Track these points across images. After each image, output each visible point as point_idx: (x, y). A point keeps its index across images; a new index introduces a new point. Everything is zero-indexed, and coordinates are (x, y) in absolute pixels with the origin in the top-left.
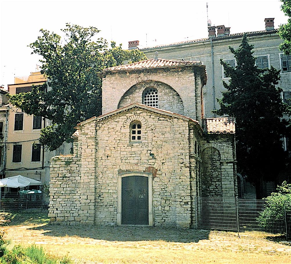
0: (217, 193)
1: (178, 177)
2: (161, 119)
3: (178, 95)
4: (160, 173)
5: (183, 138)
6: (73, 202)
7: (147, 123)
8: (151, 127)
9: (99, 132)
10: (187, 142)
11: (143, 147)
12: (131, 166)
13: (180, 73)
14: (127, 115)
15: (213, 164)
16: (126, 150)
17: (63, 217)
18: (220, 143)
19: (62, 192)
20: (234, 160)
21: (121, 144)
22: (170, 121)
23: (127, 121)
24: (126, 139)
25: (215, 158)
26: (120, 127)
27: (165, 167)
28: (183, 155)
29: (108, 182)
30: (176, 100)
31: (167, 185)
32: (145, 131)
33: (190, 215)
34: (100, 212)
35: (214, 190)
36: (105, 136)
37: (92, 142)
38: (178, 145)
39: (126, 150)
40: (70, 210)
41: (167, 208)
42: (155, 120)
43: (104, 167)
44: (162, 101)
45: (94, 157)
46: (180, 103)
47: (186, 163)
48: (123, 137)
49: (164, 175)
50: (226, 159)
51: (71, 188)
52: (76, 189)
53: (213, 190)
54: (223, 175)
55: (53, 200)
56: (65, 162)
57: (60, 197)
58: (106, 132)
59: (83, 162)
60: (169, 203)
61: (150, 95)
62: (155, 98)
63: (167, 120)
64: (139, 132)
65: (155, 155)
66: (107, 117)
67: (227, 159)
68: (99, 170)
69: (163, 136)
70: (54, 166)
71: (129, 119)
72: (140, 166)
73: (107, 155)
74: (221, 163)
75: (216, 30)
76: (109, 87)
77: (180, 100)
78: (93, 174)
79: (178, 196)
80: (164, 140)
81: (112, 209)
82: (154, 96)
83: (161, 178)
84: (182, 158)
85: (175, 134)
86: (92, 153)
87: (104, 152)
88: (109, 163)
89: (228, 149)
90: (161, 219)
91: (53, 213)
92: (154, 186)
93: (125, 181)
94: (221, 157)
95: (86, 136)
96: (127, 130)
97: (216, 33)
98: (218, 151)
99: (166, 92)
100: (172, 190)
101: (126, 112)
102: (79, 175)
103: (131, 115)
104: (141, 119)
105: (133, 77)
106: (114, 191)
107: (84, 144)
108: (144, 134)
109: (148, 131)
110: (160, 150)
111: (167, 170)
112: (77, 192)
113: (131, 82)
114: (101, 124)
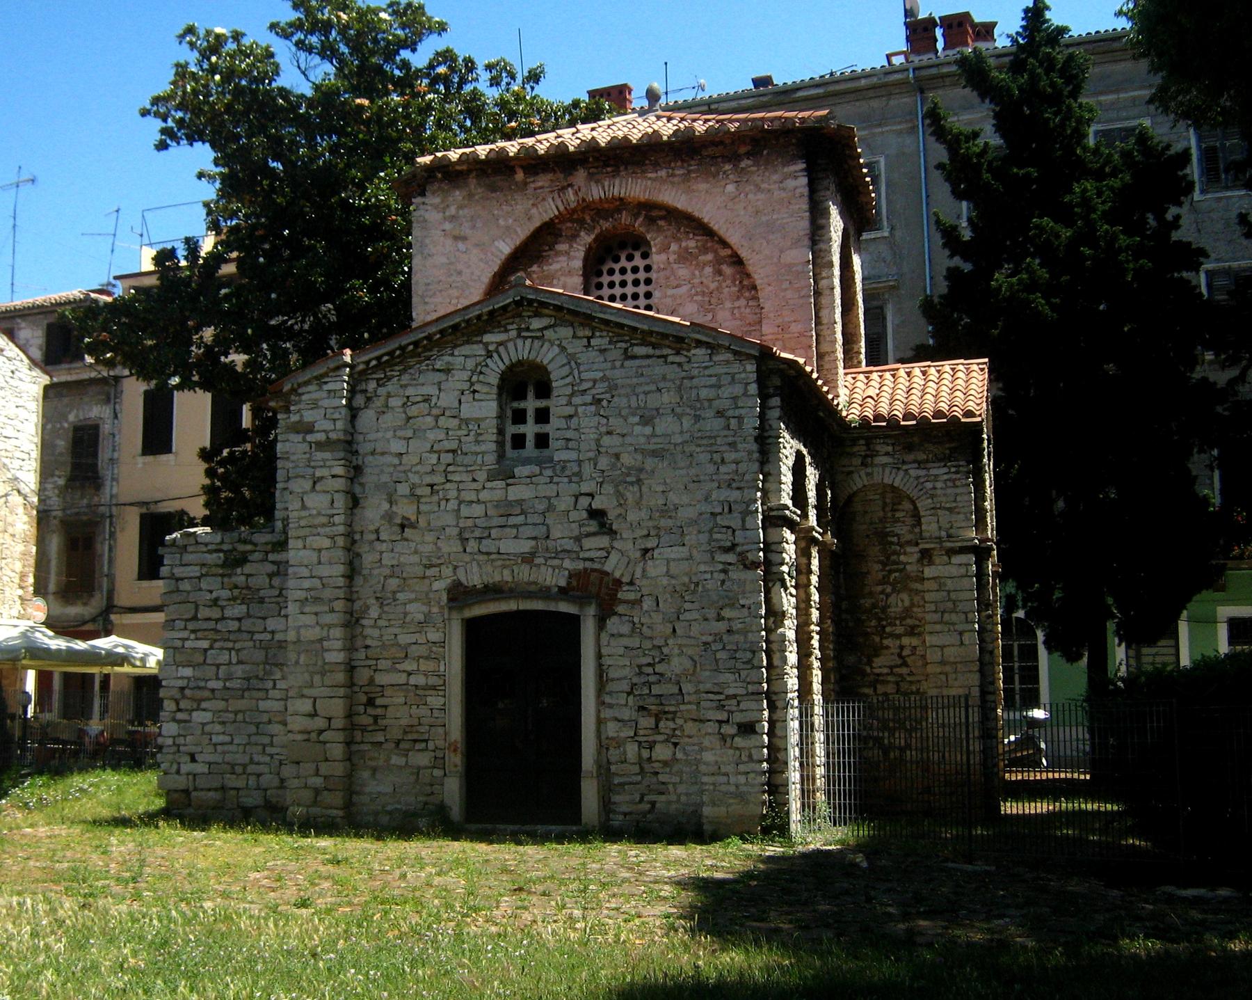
0: (904, 686)
1: (711, 614)
2: (640, 350)
3: (737, 261)
4: (632, 596)
5: (732, 433)
6: (257, 725)
7: (576, 372)
8: (594, 391)
9: (367, 418)
10: (750, 453)
11: (556, 480)
12: (504, 567)
13: (743, 165)
14: (487, 338)
15: (888, 558)
17: (216, 790)
18: (920, 464)
19: (212, 684)
21: (460, 469)
22: (678, 359)
23: (487, 366)
24: (483, 448)
25: (897, 535)
26: (456, 397)
27: (656, 569)
28: (735, 514)
29: (404, 639)
30: (729, 282)
31: (665, 650)
32: (568, 408)
34: (374, 770)
35: (892, 673)
36: (390, 434)
37: (333, 467)
39: (484, 495)
40: (247, 759)
41: (662, 752)
43: (387, 572)
44: (667, 287)
46: (747, 294)
47: (745, 548)
48: (471, 438)
49: (648, 604)
51: (247, 667)
52: (271, 673)
53: (885, 671)
55: (174, 720)
56: (221, 555)
57: (204, 705)
58: (392, 419)
59: (296, 554)
60: (674, 730)
61: (617, 267)
62: (642, 275)
63: (665, 357)
64: (543, 416)
65: (612, 515)
66: (398, 353)
67: (949, 536)
68: (366, 592)
69: (648, 430)
70: (178, 571)
71: (495, 355)
72: (543, 568)
73: (399, 521)
75: (939, 32)
76: (439, 233)
77: (745, 283)
78: (339, 605)
79: (711, 696)
80: (652, 447)
81: (423, 759)
82: (635, 270)
83: (636, 620)
84: (728, 527)
86: (335, 512)
87: (386, 506)
88: (408, 555)
90: (637, 797)
91: (178, 772)
92: (601, 651)
93: (474, 630)
94: (924, 527)
95: (309, 438)
96: (487, 408)
97: (940, 45)
98: (913, 503)
99: (686, 249)
101: (481, 324)
102: (280, 612)
103: (501, 337)
104: (550, 356)
105: (541, 188)
106: (432, 681)
107: (300, 471)
108: (562, 423)
109: (580, 410)
110: (634, 493)
111: (665, 581)
112: (275, 685)
113: (534, 211)
114: (372, 385)
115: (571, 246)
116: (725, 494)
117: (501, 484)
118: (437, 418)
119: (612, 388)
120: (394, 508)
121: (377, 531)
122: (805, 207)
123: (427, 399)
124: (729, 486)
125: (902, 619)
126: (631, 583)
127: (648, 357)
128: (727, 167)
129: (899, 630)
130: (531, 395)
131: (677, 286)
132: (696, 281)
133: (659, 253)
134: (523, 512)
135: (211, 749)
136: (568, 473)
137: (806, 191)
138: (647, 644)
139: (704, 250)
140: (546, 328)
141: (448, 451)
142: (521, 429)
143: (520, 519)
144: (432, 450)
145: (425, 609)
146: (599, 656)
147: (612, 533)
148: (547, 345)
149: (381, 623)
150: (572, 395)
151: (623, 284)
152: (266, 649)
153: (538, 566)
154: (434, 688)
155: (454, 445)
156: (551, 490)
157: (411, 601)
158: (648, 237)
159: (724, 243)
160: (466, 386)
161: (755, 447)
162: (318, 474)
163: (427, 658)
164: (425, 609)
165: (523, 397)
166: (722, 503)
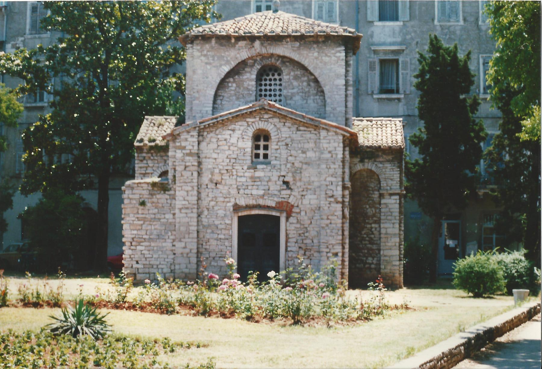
1: (325, 217)
2: (302, 128)
3: (316, 81)
4: (298, 211)
8: (286, 141)
14: (248, 120)
16: (247, 174)
20: (401, 191)
27: (306, 202)
30: (313, 89)
33: (340, 270)
36: (212, 151)
37: (192, 161)
38: (327, 170)
39: (247, 174)
42: (292, 129)
45: (196, 184)
49: (303, 213)
50: (388, 188)
54: (382, 214)
55: (130, 249)
57: (141, 244)
58: (213, 146)
61: (268, 78)
63: (310, 131)
64: (266, 148)
65: (291, 183)
69: (304, 155)
70: (131, 196)
72: (267, 200)
74: (381, 196)
82: (275, 80)
85: (322, 153)
87: (210, 176)
89: (392, 173)
95: (184, 151)
96: (248, 144)
98: (378, 176)
100: (315, 236)
106: (227, 237)
108: (273, 151)
109: (281, 147)
111: (308, 206)
113: (238, 56)
114: (205, 133)
115: (252, 70)
116: (330, 179)
117: (253, 171)
118: (229, 146)
119: (292, 140)
120: (213, 177)
121: (207, 185)
122: (344, 64)
123: (225, 140)
124: (332, 176)
125: (372, 218)
126: (298, 206)
127: (305, 131)
128: (315, 46)
129: (371, 221)
130: (262, 140)
131: (293, 89)
132: (300, 87)
133: (287, 75)
134: (260, 181)
135: (144, 259)
136: (276, 168)
137: (344, 58)
138: (302, 227)
139: (304, 75)
140: (269, 118)
141: (233, 158)
142: (258, 152)
143: (259, 183)
144: (227, 158)
145: (224, 212)
146: (286, 230)
147: (290, 189)
148: (270, 124)
149: (208, 217)
150: (278, 141)
151: (270, 85)
152: (165, 225)
153: (265, 199)
154: (227, 239)
155: (235, 156)
156: (270, 174)
157: (219, 209)
158: (282, 69)
159: (312, 74)
160: (240, 136)
161: (341, 164)
162: (187, 164)
163: (225, 229)
164: (224, 212)
165: (259, 140)
166: (329, 182)
